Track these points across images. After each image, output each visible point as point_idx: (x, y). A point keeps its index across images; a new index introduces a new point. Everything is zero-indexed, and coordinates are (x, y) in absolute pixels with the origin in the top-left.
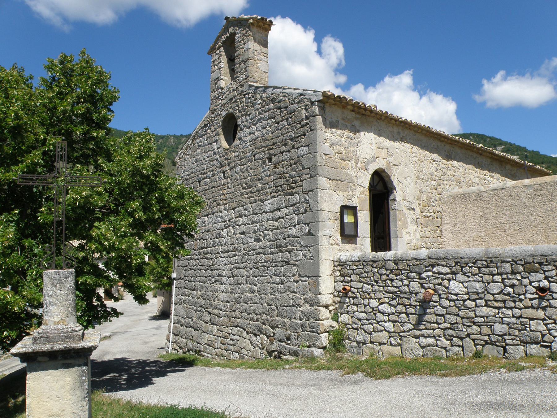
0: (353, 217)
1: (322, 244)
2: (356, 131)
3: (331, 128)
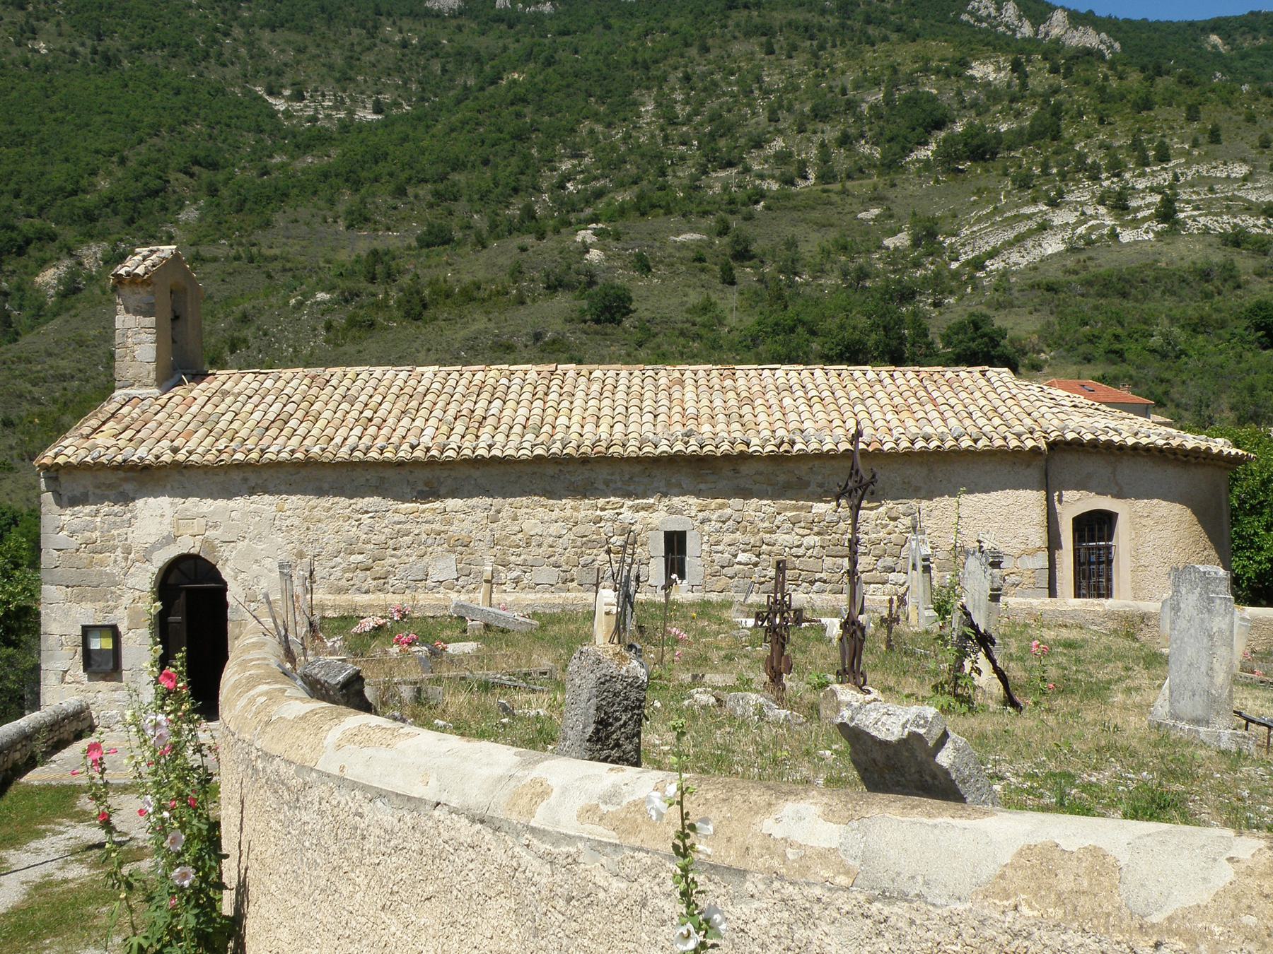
0: (111, 640)
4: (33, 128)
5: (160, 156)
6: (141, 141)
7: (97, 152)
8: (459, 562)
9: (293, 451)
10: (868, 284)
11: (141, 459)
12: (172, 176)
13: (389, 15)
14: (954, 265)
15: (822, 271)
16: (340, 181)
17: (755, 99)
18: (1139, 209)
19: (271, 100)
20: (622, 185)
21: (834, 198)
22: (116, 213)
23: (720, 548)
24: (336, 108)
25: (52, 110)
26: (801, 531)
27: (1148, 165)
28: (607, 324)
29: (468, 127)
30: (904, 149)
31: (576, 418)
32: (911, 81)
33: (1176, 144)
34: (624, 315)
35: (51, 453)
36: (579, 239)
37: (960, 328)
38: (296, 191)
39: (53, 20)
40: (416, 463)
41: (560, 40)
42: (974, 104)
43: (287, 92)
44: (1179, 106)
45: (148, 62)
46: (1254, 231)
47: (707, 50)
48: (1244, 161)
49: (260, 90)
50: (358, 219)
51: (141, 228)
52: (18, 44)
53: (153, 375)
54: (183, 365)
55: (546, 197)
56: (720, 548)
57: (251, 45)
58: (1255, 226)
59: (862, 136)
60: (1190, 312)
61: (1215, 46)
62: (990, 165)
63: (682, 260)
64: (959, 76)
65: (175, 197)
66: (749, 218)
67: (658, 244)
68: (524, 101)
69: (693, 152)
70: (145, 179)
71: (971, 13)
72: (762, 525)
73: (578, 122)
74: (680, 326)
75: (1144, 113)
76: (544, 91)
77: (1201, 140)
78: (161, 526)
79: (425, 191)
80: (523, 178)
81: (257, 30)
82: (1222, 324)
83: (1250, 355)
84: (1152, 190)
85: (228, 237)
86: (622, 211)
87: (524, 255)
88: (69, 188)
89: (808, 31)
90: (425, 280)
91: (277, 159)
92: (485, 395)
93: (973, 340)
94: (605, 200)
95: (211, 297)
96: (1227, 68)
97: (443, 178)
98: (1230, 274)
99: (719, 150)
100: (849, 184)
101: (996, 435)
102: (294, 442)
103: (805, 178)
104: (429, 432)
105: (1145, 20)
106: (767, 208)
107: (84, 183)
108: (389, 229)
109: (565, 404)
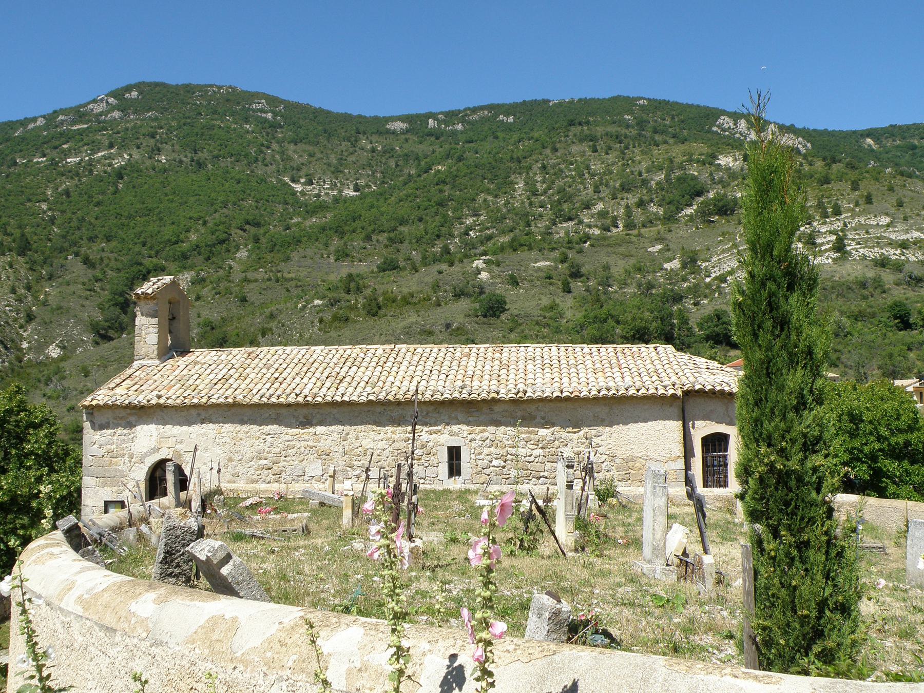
2: (131, 425)
4: (155, 205)
5: (227, 219)
6: (216, 211)
7: (190, 218)
8: (323, 464)
9: (226, 398)
10: (654, 291)
11: (139, 402)
12: (233, 231)
13: (365, 133)
14: (708, 280)
15: (626, 284)
16: (332, 232)
17: (586, 179)
18: (823, 244)
19: (293, 185)
20: (504, 233)
21: (634, 239)
22: (199, 254)
23: (481, 457)
24: (331, 189)
25: (166, 195)
26: (532, 447)
27: (828, 217)
28: (492, 318)
29: (410, 199)
30: (677, 208)
31: (399, 377)
32: (681, 167)
33: (845, 204)
34: (501, 312)
35: (89, 399)
36: (474, 265)
37: (709, 319)
38: (305, 239)
39: (170, 143)
40: (297, 405)
41: (466, 146)
42: (721, 181)
43: (303, 180)
44: (846, 181)
45: (222, 165)
46: (894, 257)
47: (557, 150)
48: (887, 214)
49: (287, 179)
50: (343, 255)
51: (213, 263)
52: (150, 158)
53: (156, 352)
54: (175, 346)
55: (457, 240)
56: (481, 457)
57: (282, 153)
58: (895, 254)
59: (652, 201)
60: (853, 308)
61: (869, 145)
62: (730, 218)
63: (538, 278)
64: (711, 164)
65: (234, 244)
66: (580, 252)
67: (523, 268)
68: (444, 182)
69: (548, 212)
70: (217, 233)
71: (718, 126)
72: (507, 443)
73: (477, 195)
74: (536, 318)
75: (825, 186)
76: (457, 176)
77: (860, 202)
78: (149, 441)
79: (383, 238)
80: (443, 229)
81: (286, 144)
82: (873, 315)
83: (891, 334)
84: (831, 232)
85: (264, 267)
86: (502, 249)
87: (441, 276)
88: (174, 239)
89: (618, 138)
90: (380, 292)
91: (295, 220)
92: (349, 364)
93: (717, 326)
94: (492, 241)
95: (253, 303)
96: (877, 158)
97: (394, 229)
98: (878, 283)
99: (563, 210)
100: (643, 230)
101: (652, 386)
102: (230, 392)
103: (617, 227)
104: (310, 386)
105: (826, 129)
106: (592, 245)
107: (182, 236)
108: (361, 261)
109: (395, 369)
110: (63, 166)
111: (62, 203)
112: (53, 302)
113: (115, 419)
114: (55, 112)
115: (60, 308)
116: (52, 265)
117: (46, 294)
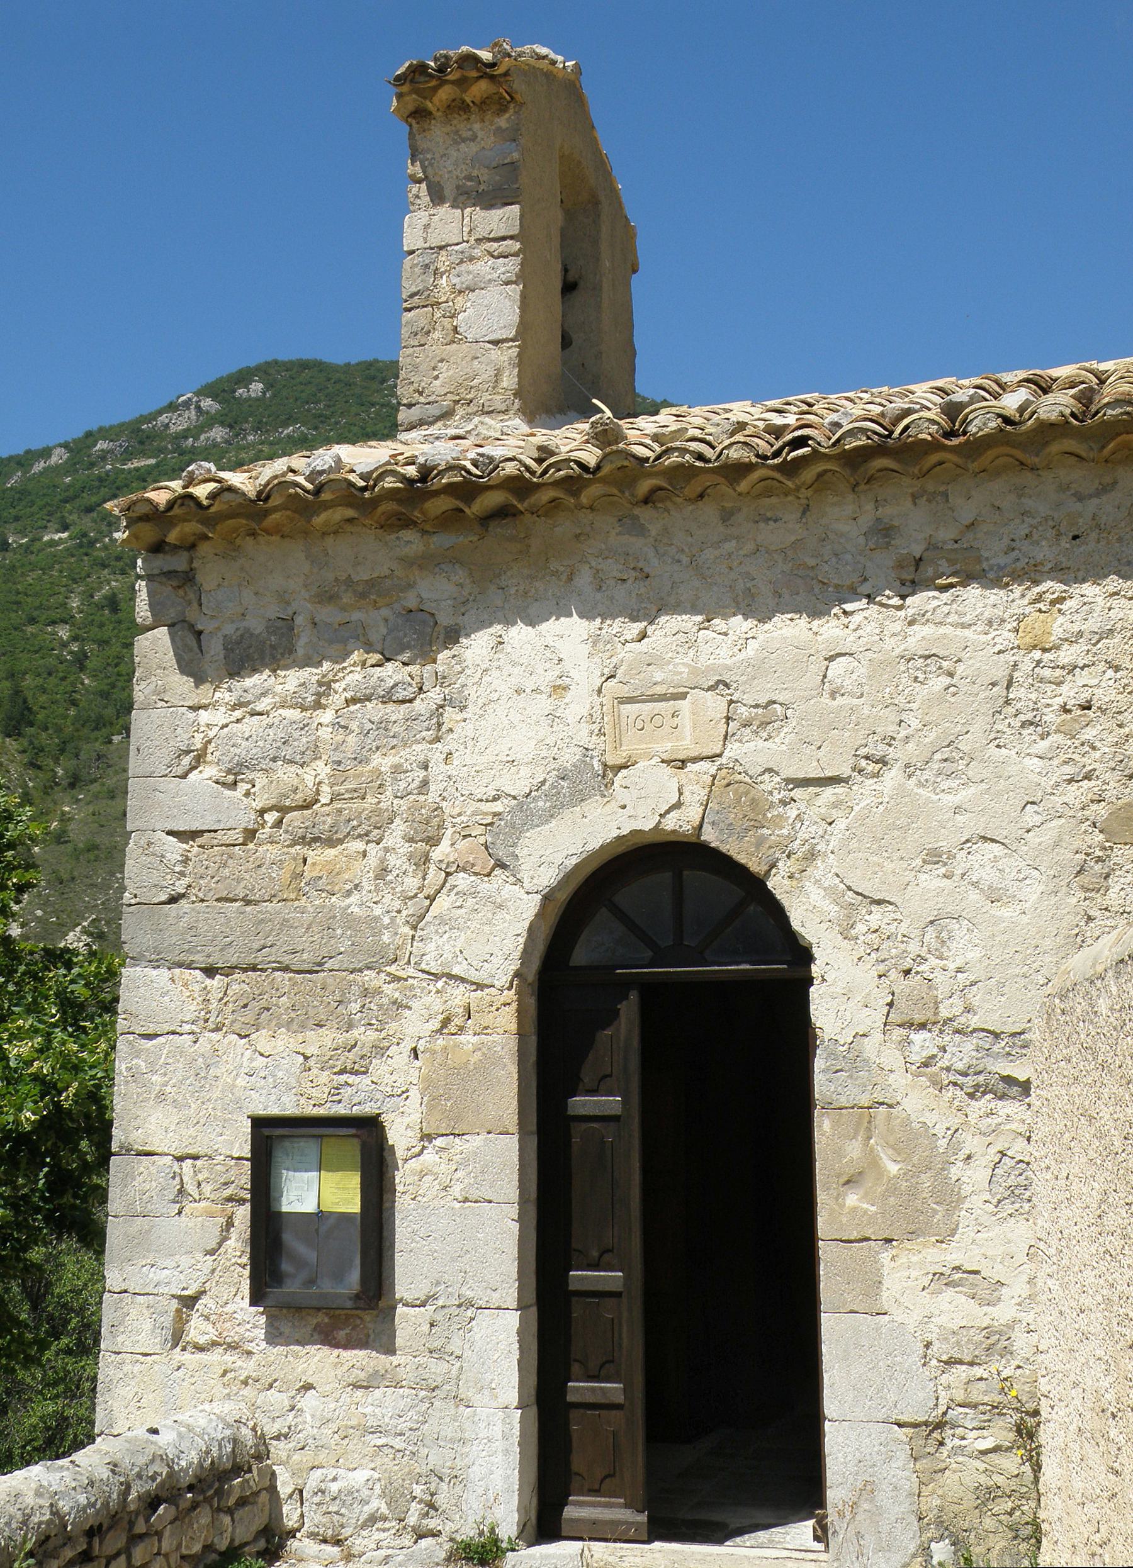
1: (123, 1341)
2: (425, 634)
3: (231, 675)
53: (509, 380)
110: (105, 548)
111: (101, 625)
112: (78, 834)
113: (327, 597)
114: (89, 434)
115: (92, 847)
116: (77, 756)
117: (64, 819)
